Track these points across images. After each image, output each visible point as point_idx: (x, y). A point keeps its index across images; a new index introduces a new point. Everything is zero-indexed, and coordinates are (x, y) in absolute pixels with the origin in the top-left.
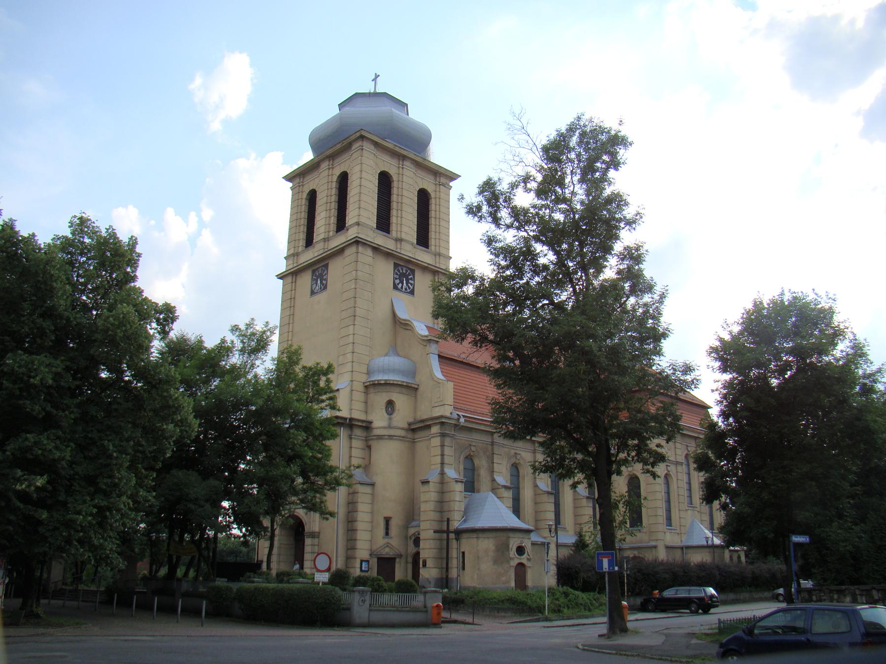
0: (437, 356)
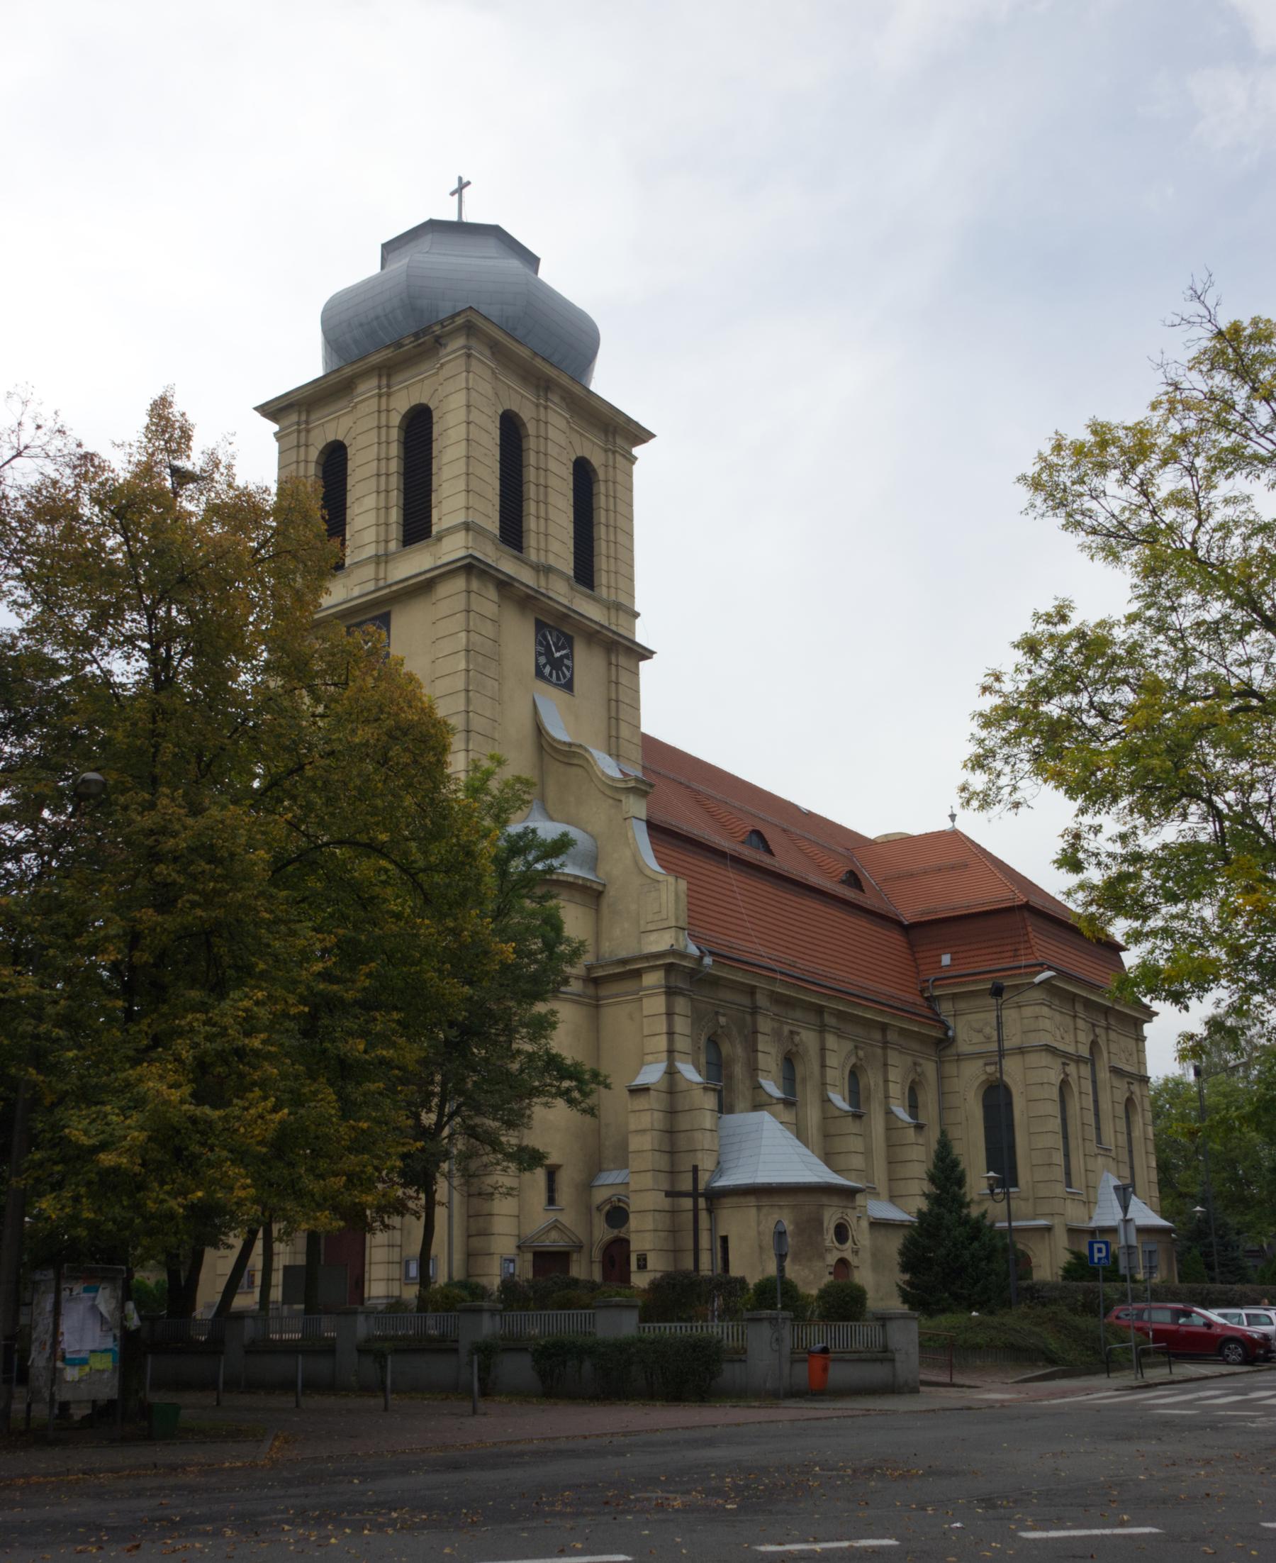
0: (643, 826)
